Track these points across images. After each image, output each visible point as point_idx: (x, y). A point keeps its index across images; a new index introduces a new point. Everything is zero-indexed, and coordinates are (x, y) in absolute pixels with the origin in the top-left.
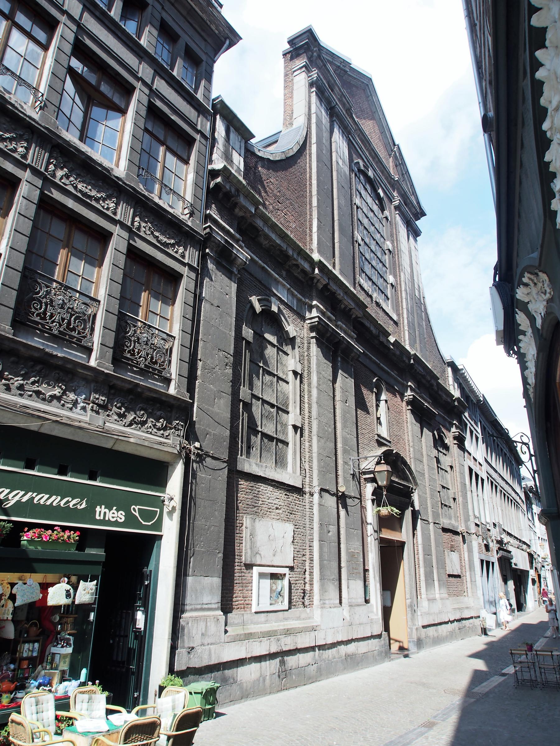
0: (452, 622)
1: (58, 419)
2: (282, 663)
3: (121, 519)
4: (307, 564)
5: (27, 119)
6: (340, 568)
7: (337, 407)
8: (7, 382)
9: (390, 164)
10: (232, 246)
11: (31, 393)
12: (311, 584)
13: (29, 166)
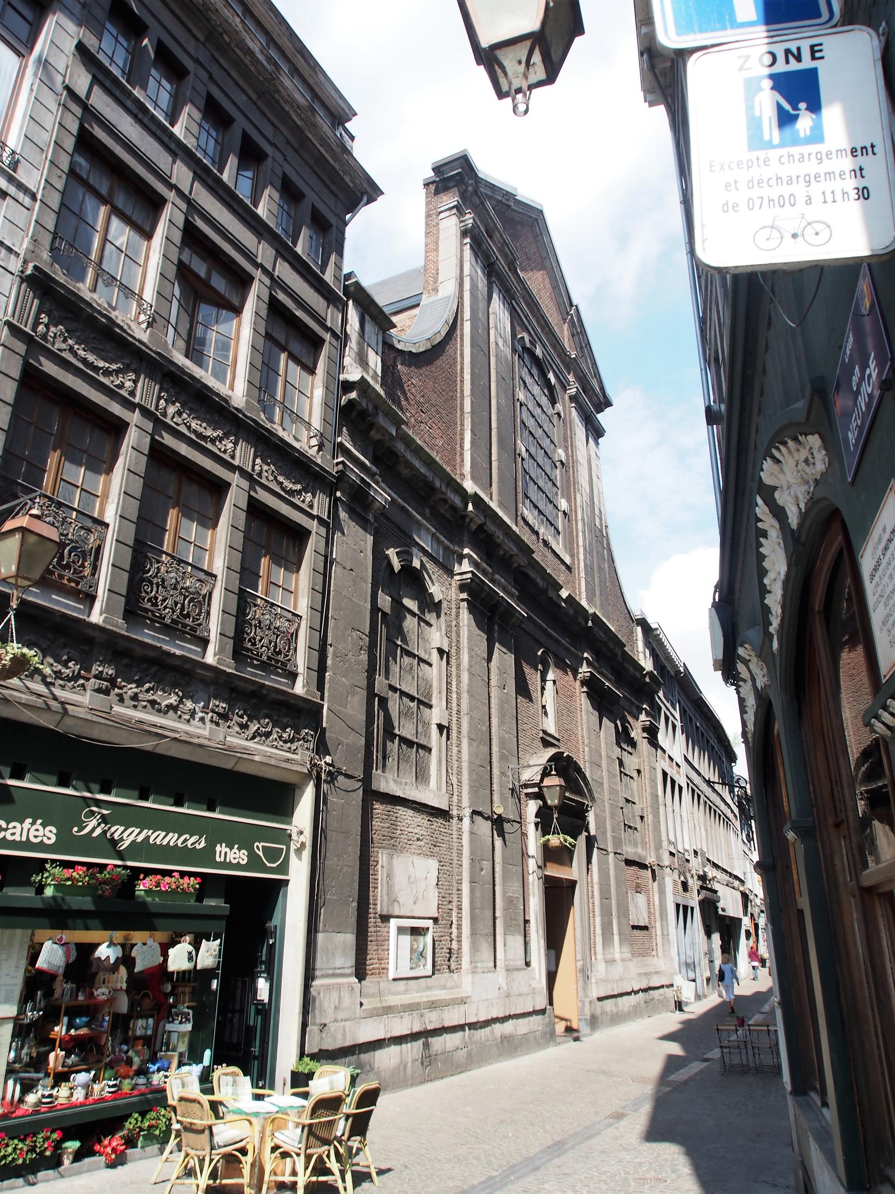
0: (636, 992)
1: (177, 736)
2: (426, 1046)
3: (49, 838)
4: (454, 914)
5: (137, 343)
6: (494, 918)
7: (492, 695)
8: (120, 691)
9: (564, 334)
10: (369, 485)
11: (145, 703)
12: (459, 942)
13: (139, 405)
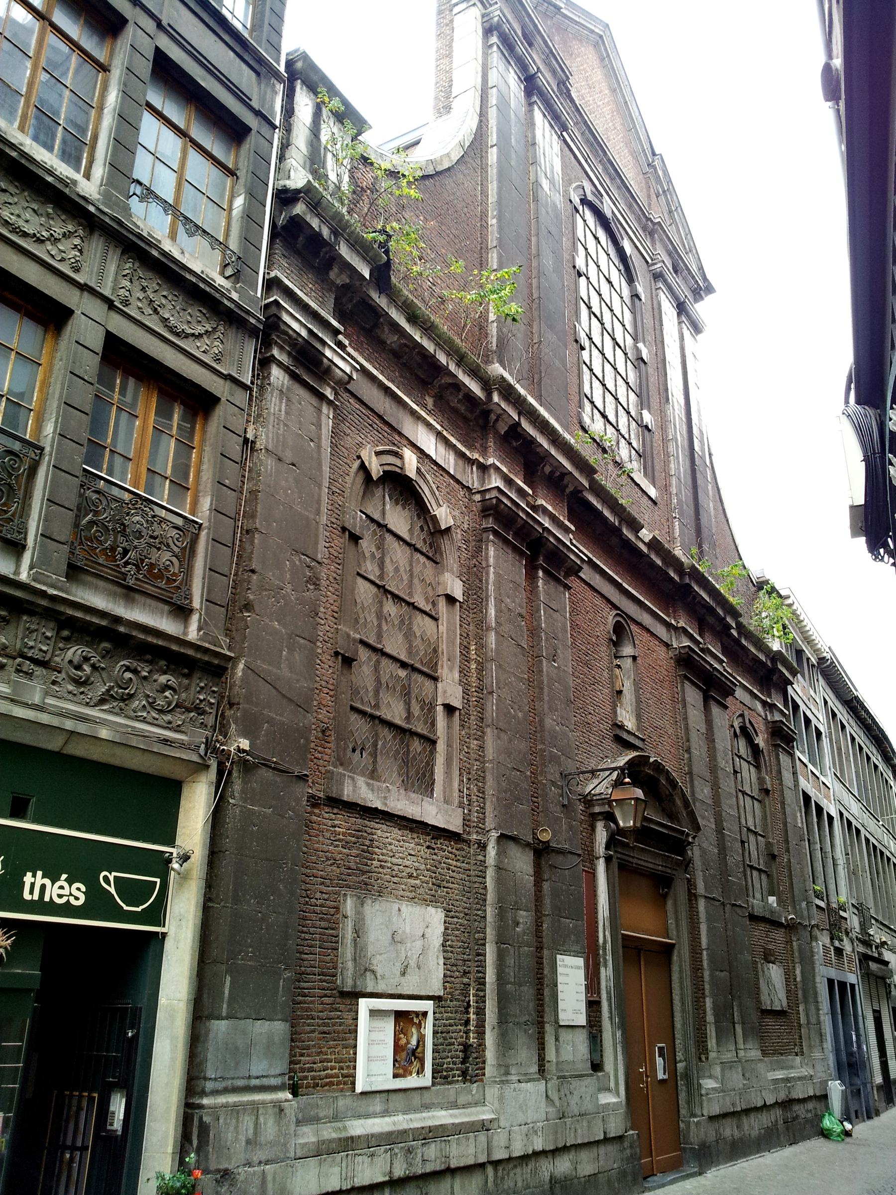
3: (77, 898)
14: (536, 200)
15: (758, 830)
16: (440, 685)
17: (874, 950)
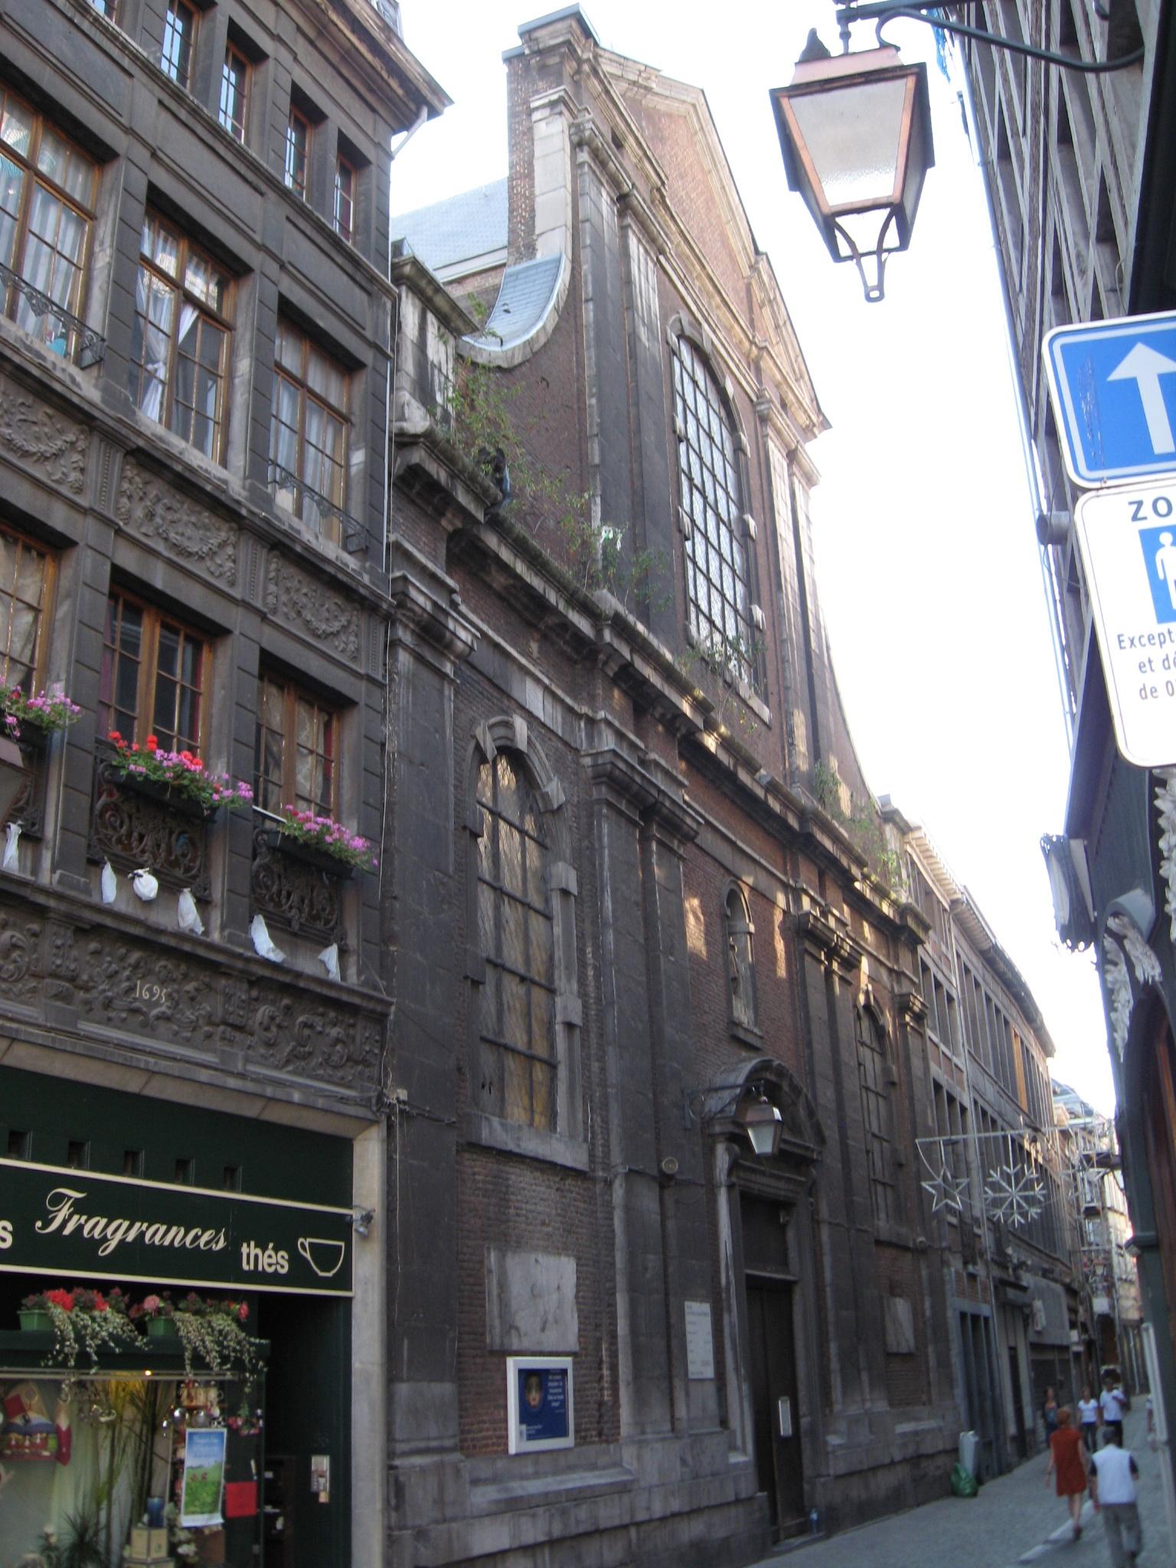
3: (282, 1267)
14: (633, 355)
15: (883, 1134)
16: (558, 1000)
17: (1011, 1271)
